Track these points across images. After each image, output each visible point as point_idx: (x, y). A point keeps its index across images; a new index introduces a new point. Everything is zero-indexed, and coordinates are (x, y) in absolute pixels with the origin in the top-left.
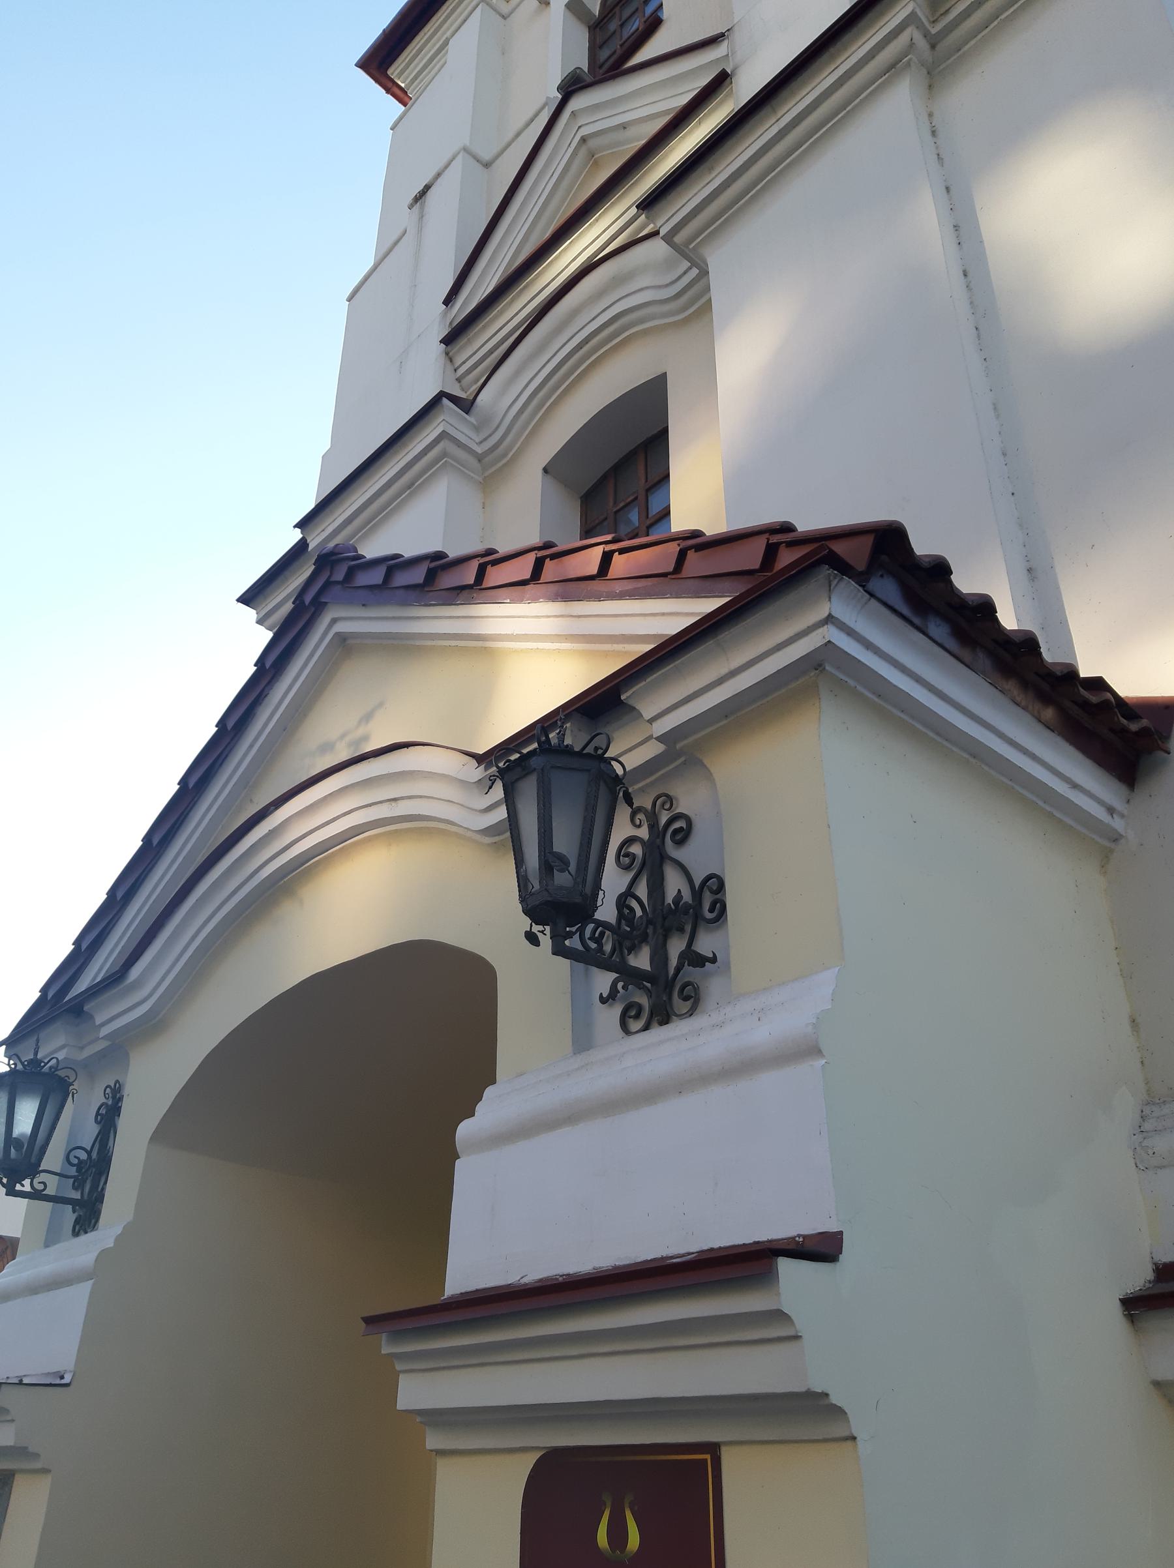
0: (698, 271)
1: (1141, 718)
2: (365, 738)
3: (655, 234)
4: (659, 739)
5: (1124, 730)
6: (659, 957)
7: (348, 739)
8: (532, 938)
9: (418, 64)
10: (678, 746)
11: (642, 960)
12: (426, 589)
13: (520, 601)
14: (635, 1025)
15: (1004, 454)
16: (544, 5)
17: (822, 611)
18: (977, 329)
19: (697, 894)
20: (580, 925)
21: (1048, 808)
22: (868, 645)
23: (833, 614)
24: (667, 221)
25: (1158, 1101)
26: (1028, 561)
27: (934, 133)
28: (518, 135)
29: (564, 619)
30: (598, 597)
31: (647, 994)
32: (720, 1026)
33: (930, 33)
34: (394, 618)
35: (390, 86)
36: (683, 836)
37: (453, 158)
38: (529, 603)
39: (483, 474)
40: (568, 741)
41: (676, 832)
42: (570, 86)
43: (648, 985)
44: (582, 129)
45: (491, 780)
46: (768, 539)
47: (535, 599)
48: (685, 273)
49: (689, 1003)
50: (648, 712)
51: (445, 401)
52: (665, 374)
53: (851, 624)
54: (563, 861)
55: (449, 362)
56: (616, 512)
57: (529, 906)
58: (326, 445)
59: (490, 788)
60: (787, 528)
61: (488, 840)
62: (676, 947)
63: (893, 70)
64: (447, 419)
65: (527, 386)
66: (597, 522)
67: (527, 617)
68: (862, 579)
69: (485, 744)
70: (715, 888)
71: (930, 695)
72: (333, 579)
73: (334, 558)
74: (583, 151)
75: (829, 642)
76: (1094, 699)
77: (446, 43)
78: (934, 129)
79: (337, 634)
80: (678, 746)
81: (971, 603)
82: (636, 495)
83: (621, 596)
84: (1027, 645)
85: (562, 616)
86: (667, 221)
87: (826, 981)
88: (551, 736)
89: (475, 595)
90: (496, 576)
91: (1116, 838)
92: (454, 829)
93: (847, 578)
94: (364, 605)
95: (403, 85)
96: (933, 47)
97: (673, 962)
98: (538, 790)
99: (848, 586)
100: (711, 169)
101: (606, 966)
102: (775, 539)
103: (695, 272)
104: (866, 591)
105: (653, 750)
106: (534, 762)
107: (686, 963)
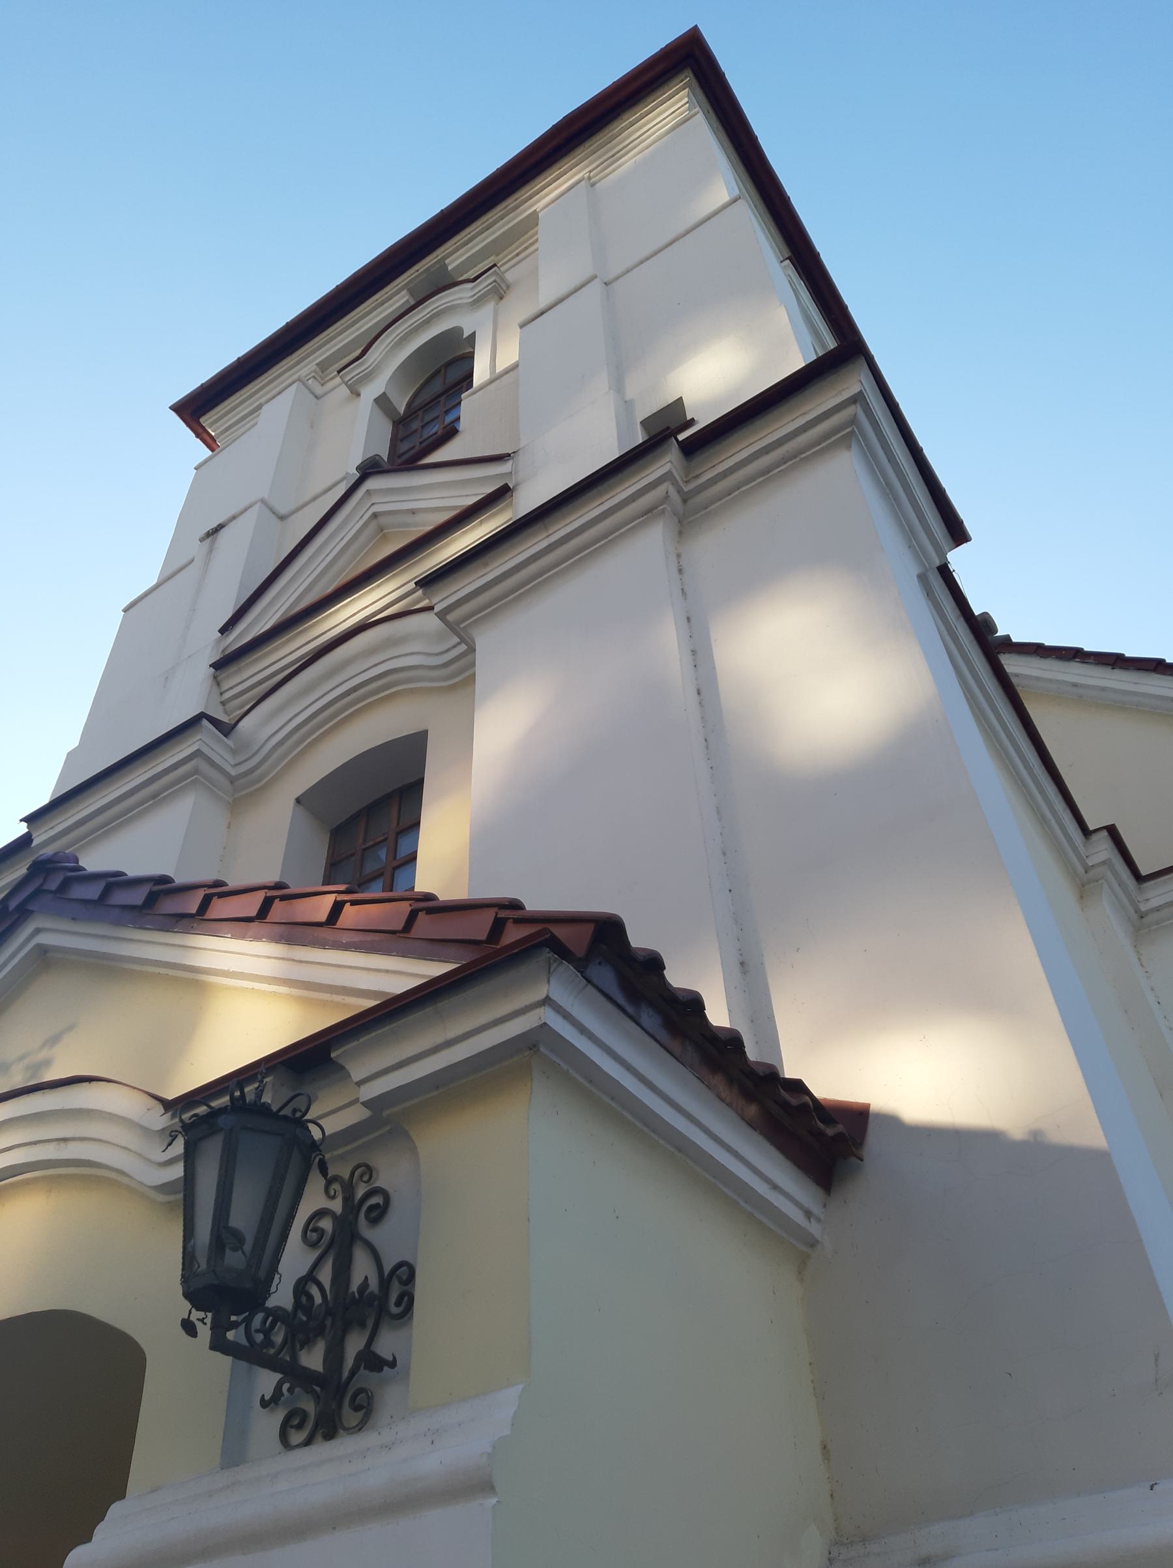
0: (466, 647)
1: (837, 1123)
2: (47, 1063)
3: (430, 608)
4: (365, 1104)
5: (821, 1134)
6: (334, 1356)
7: (26, 1061)
8: (189, 1327)
9: (231, 418)
10: (386, 1113)
11: (313, 1359)
12: (145, 911)
13: (243, 937)
14: (296, 1437)
15: (724, 854)
16: (355, 396)
17: (540, 992)
18: (706, 740)
19: (385, 1282)
20: (247, 1314)
21: (749, 1209)
22: (583, 1030)
23: (551, 996)
24: (443, 600)
25: (845, 1541)
26: (741, 955)
27: (680, 571)
28: (315, 498)
29: (285, 962)
30: (323, 945)
31: (315, 1401)
32: (388, 1447)
33: (683, 490)
34: (104, 937)
35: (201, 433)
36: (378, 1214)
37: (250, 506)
38: (251, 941)
39: (233, 795)
40: (267, 1098)
41: (372, 1208)
42: (369, 468)
43: (318, 1389)
44: (376, 506)
45: (171, 1136)
46: (497, 914)
47: (257, 938)
48: (454, 647)
49: (360, 1414)
50: (357, 1073)
51: (205, 722)
52: (426, 731)
53: (568, 1009)
54: (238, 1237)
55: (216, 685)
56: (365, 850)
57: (191, 1289)
58: (74, 742)
59: (170, 1144)
60: (516, 905)
61: (161, 1198)
62: (354, 1344)
63: (650, 514)
64: (204, 740)
65: (290, 720)
66: (344, 856)
67: (247, 955)
68: (581, 965)
69: (174, 1090)
70: (404, 1278)
71: (642, 1086)
72: (45, 887)
73: (51, 866)
74: (373, 525)
75: (545, 1023)
76: (794, 1101)
77: (260, 407)
78: (680, 568)
79: (39, 946)
80: (386, 1113)
81: (681, 998)
82: (386, 836)
83: (346, 947)
84: (731, 1043)
85: (283, 959)
86: (443, 600)
87: (509, 1398)
88: (246, 1090)
89: (195, 925)
90: (220, 908)
91: (813, 1243)
92: (125, 1180)
93: (566, 963)
94: (73, 919)
95: (213, 434)
96: (685, 501)
97: (349, 1362)
98: (222, 1156)
99: (566, 970)
100: (487, 565)
101: (271, 1364)
102: (503, 914)
103: (463, 647)
104: (583, 976)
105: (354, 1116)
106: (222, 1121)
107: (363, 1365)
